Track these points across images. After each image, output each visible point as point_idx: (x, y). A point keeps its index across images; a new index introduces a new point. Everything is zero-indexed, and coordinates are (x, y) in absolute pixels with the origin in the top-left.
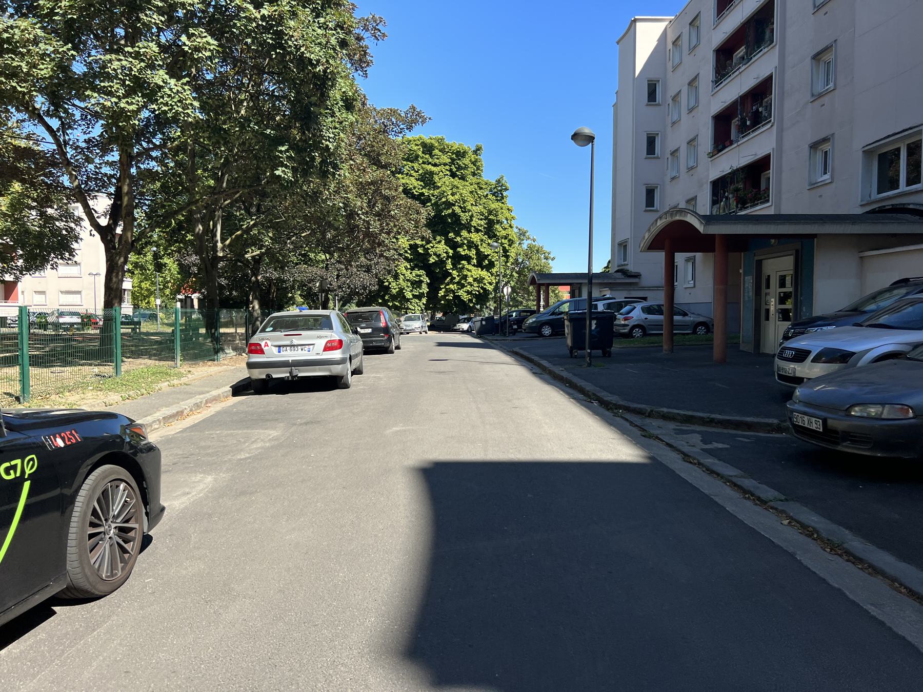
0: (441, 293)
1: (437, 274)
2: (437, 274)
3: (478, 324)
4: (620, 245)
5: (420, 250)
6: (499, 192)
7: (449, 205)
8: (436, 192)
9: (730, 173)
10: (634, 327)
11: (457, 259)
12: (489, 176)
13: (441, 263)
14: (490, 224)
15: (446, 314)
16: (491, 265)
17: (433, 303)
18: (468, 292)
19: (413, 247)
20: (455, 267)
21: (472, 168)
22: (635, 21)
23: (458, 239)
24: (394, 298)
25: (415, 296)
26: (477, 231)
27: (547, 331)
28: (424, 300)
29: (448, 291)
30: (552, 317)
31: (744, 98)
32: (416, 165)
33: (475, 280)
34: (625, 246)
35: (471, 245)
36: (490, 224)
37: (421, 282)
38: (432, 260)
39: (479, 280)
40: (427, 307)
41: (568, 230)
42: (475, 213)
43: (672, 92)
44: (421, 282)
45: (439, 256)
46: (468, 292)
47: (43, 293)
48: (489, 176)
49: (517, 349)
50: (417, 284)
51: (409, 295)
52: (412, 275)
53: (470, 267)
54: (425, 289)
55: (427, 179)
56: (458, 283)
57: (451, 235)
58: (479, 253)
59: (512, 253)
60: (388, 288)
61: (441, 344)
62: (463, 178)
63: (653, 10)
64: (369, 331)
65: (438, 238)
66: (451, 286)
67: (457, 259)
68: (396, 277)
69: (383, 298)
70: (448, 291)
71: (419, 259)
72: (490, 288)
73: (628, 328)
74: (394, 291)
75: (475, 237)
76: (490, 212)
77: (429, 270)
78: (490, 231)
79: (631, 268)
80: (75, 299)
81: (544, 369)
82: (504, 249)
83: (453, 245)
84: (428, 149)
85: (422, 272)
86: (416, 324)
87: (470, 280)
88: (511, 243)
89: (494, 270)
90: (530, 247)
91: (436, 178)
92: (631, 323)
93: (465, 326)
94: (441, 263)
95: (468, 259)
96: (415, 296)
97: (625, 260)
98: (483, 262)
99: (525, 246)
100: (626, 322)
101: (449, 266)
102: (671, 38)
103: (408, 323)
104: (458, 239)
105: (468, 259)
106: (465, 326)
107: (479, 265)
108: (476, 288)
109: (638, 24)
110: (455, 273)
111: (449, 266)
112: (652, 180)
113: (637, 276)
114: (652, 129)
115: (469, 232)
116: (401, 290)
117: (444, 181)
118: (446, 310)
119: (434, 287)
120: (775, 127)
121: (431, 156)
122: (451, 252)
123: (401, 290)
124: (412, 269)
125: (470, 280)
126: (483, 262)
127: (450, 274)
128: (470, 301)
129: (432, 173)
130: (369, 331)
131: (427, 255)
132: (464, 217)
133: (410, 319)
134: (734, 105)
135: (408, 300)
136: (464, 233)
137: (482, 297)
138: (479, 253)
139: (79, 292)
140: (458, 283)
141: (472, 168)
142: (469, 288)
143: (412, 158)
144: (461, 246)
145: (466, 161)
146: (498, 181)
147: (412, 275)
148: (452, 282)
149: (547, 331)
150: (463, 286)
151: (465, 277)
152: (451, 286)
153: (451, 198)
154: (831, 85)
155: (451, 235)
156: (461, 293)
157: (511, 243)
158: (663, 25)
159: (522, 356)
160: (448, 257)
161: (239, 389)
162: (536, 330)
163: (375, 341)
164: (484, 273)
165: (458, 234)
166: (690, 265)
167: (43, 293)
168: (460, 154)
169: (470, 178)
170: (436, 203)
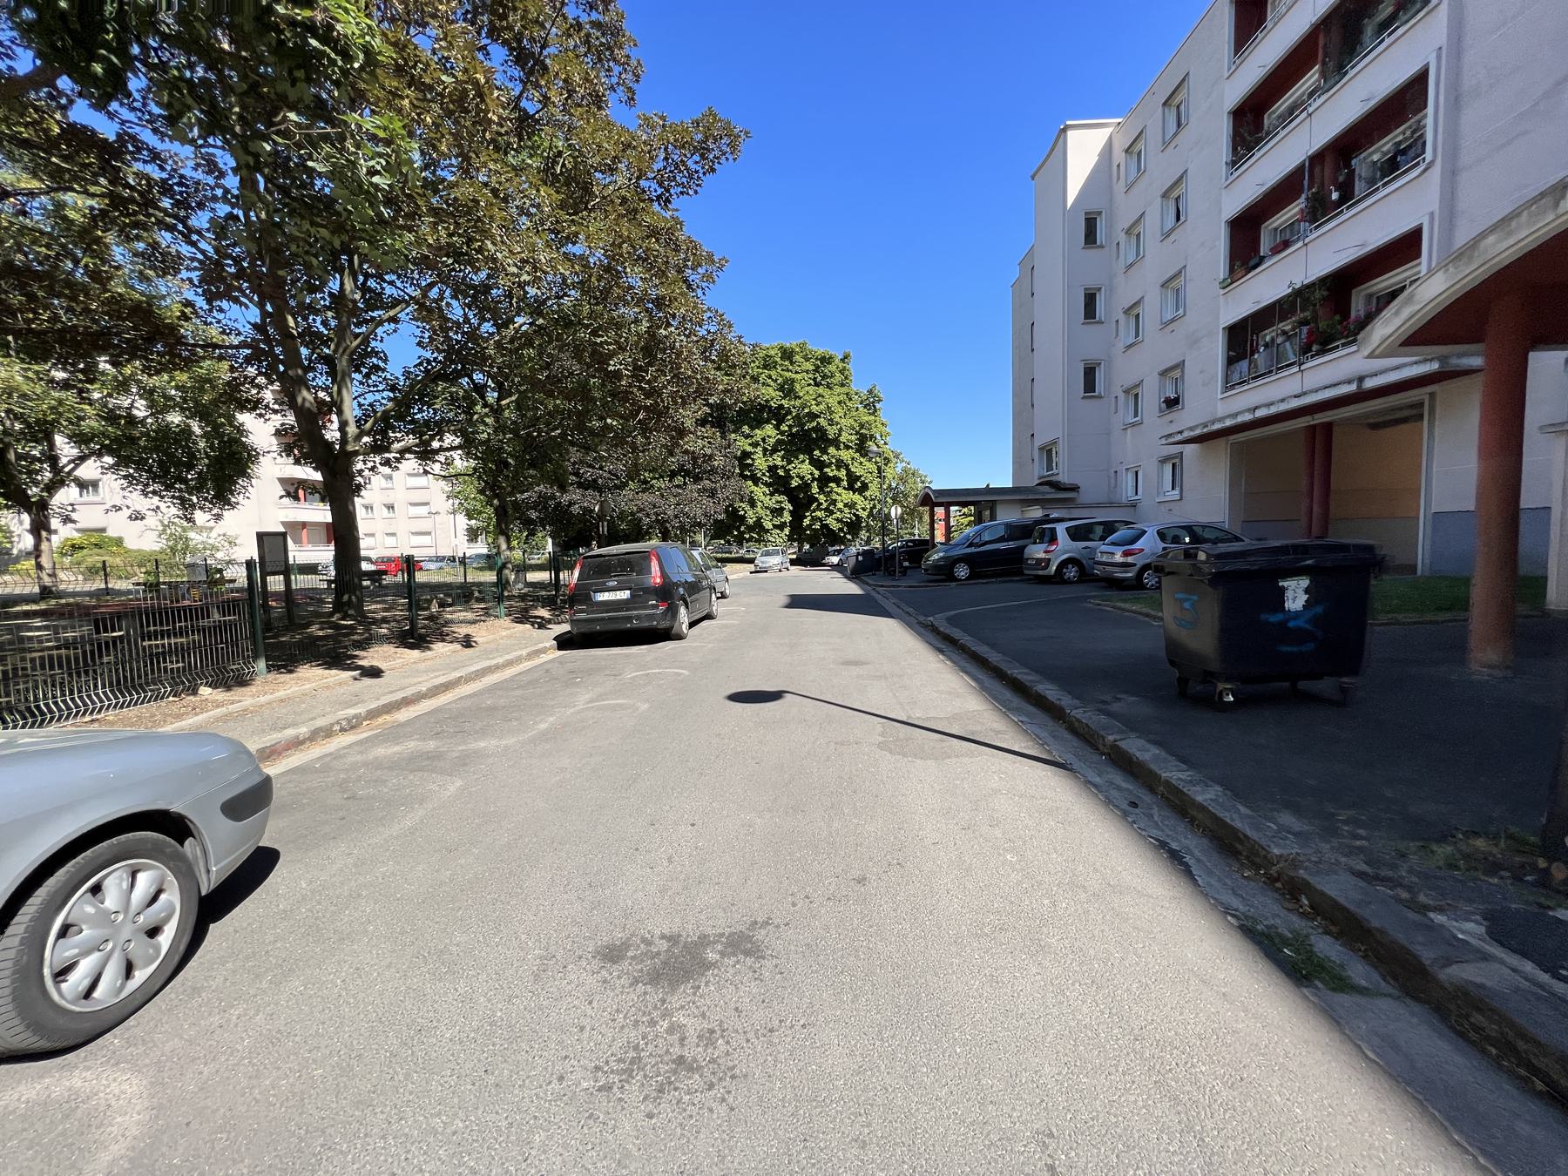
0: (806, 522)
1: (801, 500)
2: (801, 500)
3: (852, 561)
4: (1041, 449)
5: (781, 472)
6: (871, 405)
7: (813, 416)
8: (798, 402)
9: (1289, 296)
10: (1146, 567)
11: (824, 481)
12: (859, 386)
13: (805, 486)
14: (863, 439)
15: (813, 547)
16: (865, 487)
17: (797, 532)
18: (838, 520)
19: (772, 469)
20: (821, 489)
21: (839, 377)
22: (1064, 130)
23: (825, 457)
24: (750, 529)
25: (775, 526)
26: (847, 447)
27: (962, 571)
28: (787, 531)
29: (814, 519)
30: (969, 550)
31: (1317, 159)
32: (773, 373)
33: (846, 505)
34: (1049, 452)
35: (840, 464)
36: (863, 439)
37: (782, 509)
38: (794, 484)
39: (851, 506)
40: (790, 538)
41: (951, 444)
42: (843, 425)
43: (1125, 221)
44: (782, 509)
45: (802, 478)
46: (838, 520)
47: (393, 534)
48: (859, 386)
49: (939, 620)
50: (778, 512)
51: (768, 525)
52: (772, 502)
53: (840, 490)
54: (787, 517)
55: (788, 389)
56: (826, 509)
57: (817, 453)
58: (849, 474)
59: (889, 472)
60: (743, 517)
61: (797, 602)
62: (828, 386)
63: (1092, 109)
64: (625, 595)
65: (801, 457)
66: (818, 513)
67: (824, 481)
68: (752, 503)
69: (738, 529)
70: (814, 519)
71: (779, 483)
72: (864, 514)
73: (1136, 568)
74: (751, 522)
75: (845, 455)
76: (862, 426)
77: (791, 494)
78: (862, 449)
79: (1064, 478)
80: (426, 540)
81: (1086, 737)
82: (879, 469)
83: (819, 464)
84: (787, 354)
85: (783, 498)
86: (775, 560)
87: (840, 505)
88: (887, 461)
89: (867, 494)
90: (905, 470)
91: (797, 386)
92: (1139, 560)
93: (835, 560)
94: (805, 486)
95: (837, 480)
96: (775, 526)
97: (1049, 468)
98: (856, 484)
99: (899, 470)
100: (1130, 559)
101: (815, 490)
102: (1120, 145)
103: (764, 559)
104: (825, 457)
105: (837, 480)
106: (835, 560)
107: (851, 488)
108: (847, 515)
109: (1070, 133)
110: (822, 498)
111: (815, 490)
112: (1093, 354)
113: (1074, 488)
114: (1092, 283)
115: (838, 449)
116: (759, 519)
117: (806, 391)
118: (813, 540)
119: (797, 516)
120: (1436, 171)
121: (792, 363)
122: (817, 473)
123: (759, 519)
124: (772, 494)
125: (840, 505)
126: (856, 484)
127: (816, 500)
128: (841, 530)
129: (793, 381)
130: (625, 595)
131: (788, 477)
132: (832, 432)
133: (767, 554)
134: (1298, 173)
135: (767, 531)
136: (832, 450)
137: (854, 526)
138: (849, 474)
139: (429, 533)
140: (826, 509)
141: (839, 377)
142: (838, 515)
143: (768, 364)
144: (829, 465)
145: (832, 368)
146: (870, 392)
147: (772, 502)
148: (818, 508)
149: (962, 571)
150: (832, 513)
151: (834, 502)
152: (818, 513)
153: (815, 409)
154: (1181, 311)
155: (817, 453)
156: (829, 521)
157: (887, 461)
158: (1107, 131)
159: (999, 674)
160: (814, 479)
161: (564, 643)
162: (944, 571)
163: (638, 617)
164: (856, 498)
165: (824, 451)
166: (1168, 468)
167: (393, 534)
168: (825, 360)
169: (838, 389)
170: (798, 416)
